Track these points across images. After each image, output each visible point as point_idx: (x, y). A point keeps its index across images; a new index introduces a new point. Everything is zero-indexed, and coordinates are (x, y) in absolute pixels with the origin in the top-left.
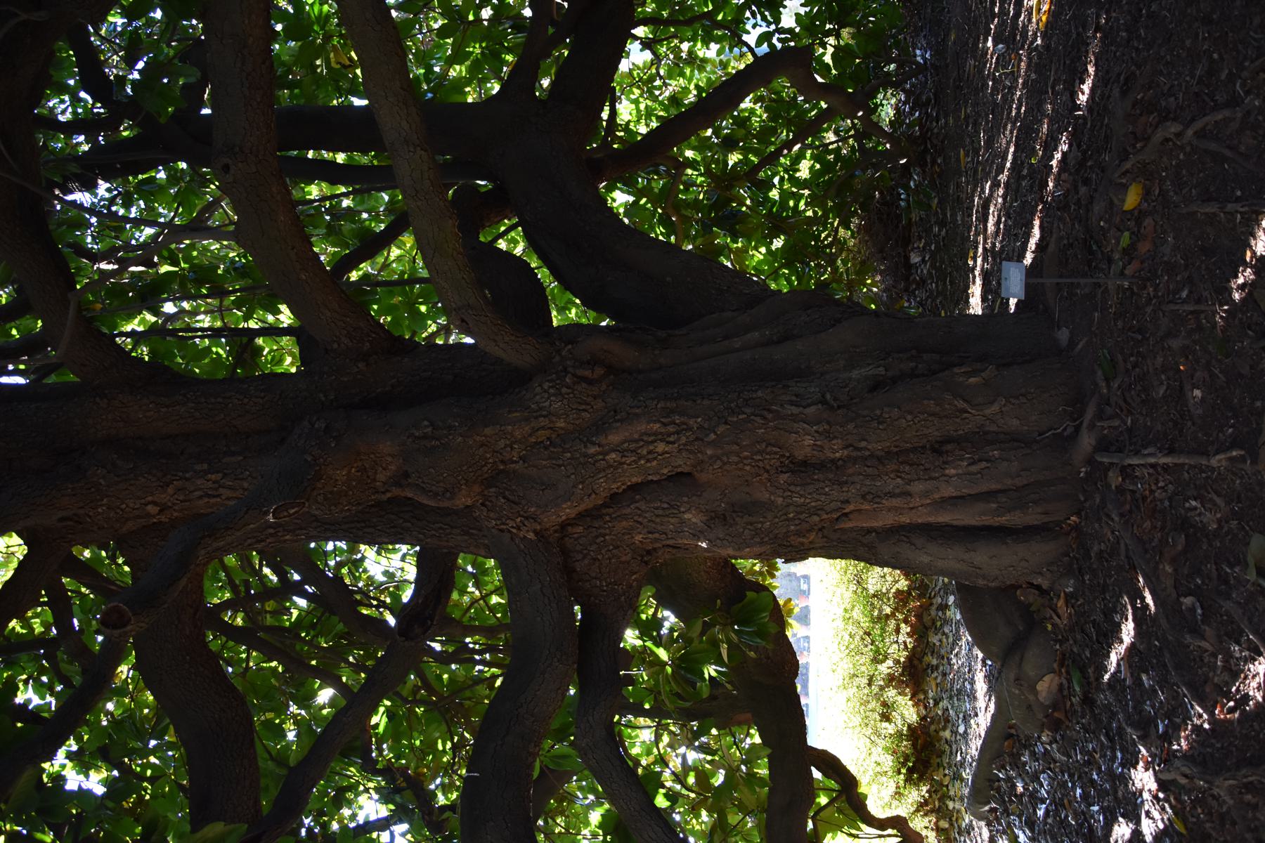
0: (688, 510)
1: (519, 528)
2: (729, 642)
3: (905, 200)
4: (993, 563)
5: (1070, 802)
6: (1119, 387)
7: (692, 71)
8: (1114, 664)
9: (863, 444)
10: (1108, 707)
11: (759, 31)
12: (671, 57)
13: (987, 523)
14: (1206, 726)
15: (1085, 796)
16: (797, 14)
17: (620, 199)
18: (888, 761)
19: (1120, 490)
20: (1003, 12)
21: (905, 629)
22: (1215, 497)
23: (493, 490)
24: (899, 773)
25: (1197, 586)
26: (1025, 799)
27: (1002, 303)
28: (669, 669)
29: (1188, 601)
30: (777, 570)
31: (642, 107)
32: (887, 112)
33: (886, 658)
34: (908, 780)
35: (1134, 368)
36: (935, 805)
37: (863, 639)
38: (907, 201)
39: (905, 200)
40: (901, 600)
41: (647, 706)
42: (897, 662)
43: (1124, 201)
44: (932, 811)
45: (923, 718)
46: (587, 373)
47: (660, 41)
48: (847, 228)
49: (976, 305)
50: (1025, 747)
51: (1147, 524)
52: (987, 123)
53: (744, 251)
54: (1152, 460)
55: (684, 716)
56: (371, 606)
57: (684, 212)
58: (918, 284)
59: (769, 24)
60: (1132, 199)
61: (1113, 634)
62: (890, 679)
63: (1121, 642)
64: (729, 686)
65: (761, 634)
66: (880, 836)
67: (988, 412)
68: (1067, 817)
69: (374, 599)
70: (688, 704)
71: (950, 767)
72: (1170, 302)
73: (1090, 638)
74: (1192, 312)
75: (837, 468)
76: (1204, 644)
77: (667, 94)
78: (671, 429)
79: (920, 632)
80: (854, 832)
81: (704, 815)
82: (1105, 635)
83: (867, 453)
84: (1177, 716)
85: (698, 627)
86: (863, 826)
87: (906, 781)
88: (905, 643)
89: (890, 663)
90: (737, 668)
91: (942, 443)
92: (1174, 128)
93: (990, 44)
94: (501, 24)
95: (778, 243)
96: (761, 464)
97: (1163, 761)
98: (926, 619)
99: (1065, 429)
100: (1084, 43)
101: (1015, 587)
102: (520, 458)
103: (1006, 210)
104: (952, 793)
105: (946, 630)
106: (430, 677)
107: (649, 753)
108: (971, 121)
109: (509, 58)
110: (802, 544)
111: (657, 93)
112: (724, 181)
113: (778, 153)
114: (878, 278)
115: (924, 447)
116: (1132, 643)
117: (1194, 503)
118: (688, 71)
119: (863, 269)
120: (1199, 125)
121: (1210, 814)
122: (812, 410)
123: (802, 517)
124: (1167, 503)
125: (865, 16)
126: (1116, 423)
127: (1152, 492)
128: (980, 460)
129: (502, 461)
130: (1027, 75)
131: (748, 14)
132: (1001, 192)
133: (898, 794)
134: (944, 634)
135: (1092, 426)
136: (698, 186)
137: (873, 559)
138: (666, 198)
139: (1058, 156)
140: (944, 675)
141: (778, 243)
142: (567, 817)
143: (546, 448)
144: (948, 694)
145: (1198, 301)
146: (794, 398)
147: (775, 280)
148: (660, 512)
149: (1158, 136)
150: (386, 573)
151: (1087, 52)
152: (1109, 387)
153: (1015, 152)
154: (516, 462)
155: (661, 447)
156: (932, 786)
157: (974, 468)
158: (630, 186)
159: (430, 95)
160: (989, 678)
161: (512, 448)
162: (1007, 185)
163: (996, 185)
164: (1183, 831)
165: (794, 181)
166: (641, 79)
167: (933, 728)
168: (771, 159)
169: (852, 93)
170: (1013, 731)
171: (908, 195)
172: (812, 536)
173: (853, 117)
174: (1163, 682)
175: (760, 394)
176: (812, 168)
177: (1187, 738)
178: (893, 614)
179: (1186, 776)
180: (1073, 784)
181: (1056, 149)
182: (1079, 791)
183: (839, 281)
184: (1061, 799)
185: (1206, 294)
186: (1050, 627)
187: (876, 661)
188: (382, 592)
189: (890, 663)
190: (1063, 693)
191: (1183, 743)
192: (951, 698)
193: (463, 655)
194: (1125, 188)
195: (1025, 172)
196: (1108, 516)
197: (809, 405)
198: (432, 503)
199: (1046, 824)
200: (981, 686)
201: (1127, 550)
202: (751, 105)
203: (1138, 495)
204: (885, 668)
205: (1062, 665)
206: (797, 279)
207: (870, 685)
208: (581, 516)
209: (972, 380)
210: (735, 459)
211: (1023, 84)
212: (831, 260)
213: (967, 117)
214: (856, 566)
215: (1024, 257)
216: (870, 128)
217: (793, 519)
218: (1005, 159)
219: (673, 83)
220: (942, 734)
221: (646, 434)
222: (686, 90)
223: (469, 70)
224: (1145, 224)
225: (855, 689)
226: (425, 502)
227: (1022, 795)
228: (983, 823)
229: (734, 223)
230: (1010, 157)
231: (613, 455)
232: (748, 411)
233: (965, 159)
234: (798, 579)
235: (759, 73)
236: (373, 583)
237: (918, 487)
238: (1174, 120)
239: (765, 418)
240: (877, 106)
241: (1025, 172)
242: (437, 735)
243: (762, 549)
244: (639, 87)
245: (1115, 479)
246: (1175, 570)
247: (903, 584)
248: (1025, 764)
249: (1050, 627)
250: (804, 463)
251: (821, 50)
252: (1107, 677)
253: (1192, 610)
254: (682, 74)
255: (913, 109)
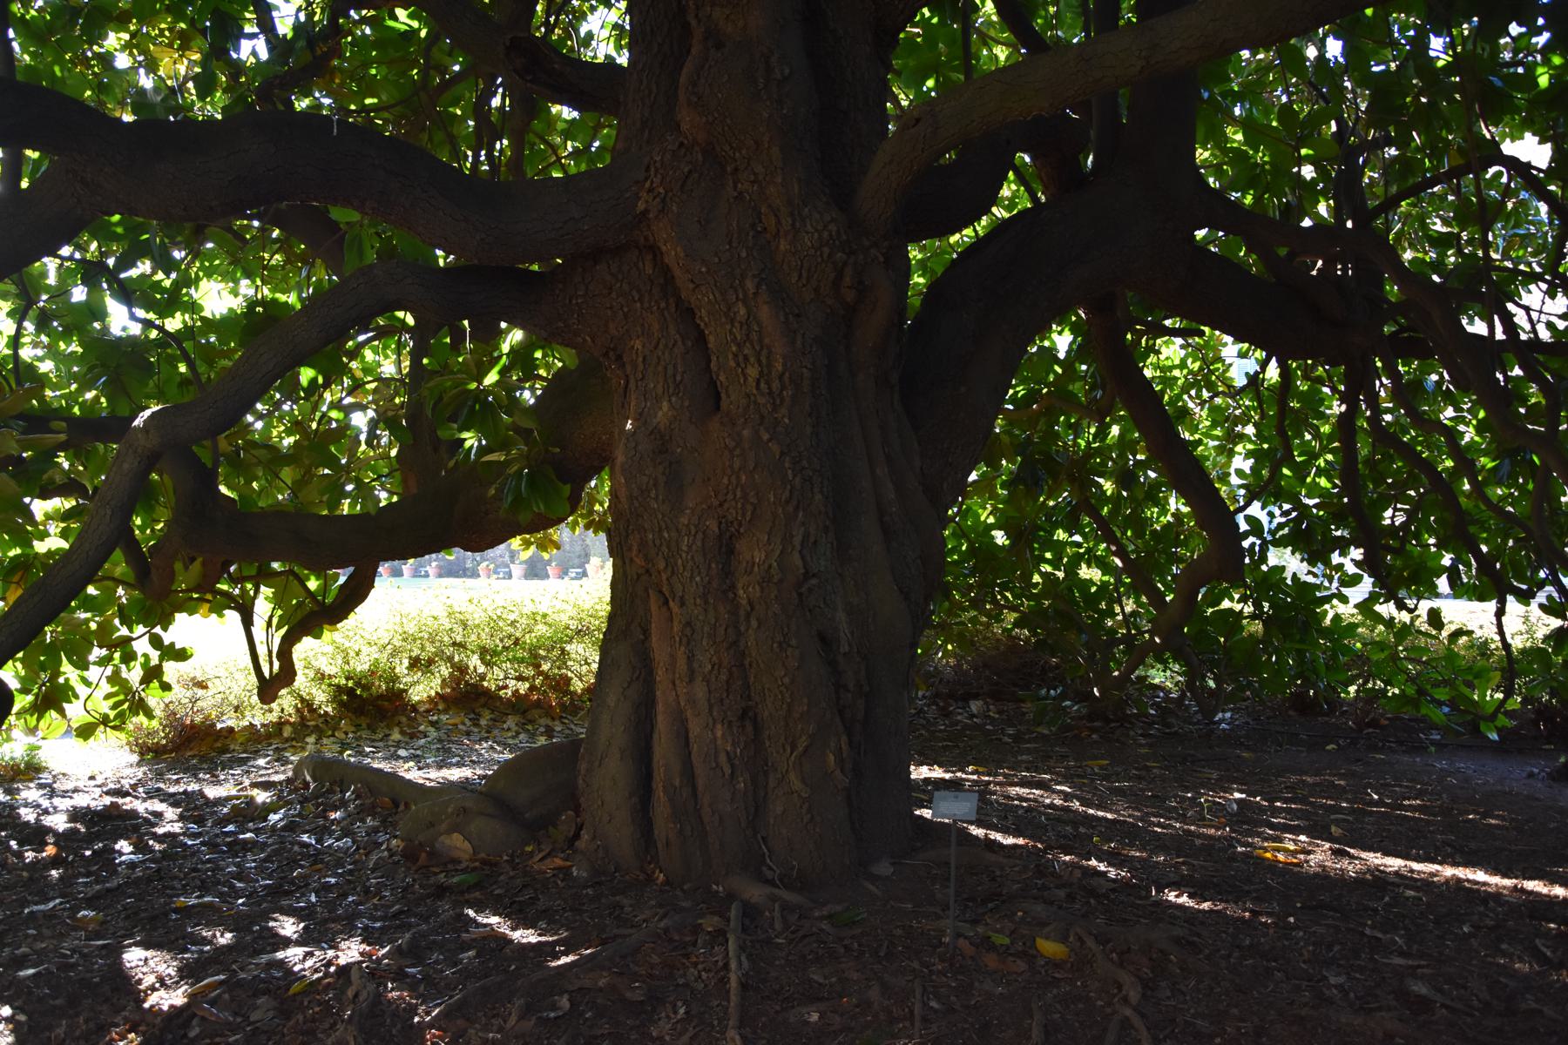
0: (672, 407)
1: (650, 191)
2: (507, 463)
3: (1051, 691)
4: (608, 783)
5: (319, 871)
6: (822, 930)
7: (1217, 438)
8: (485, 921)
9: (754, 623)
10: (435, 913)
11: (1264, 519)
12: (1237, 412)
13: (655, 774)
14: (416, 1019)
15: (327, 887)
16: (1283, 568)
17: (1062, 341)
18: (361, 666)
19: (697, 929)
20: (1276, 812)
21: (523, 687)
22: (688, 1035)
23: (700, 157)
24: (347, 679)
25: (582, 1014)
26: (321, 822)
27: (922, 800)
28: (473, 386)
29: (565, 1003)
30: (595, 532)
31: (1176, 373)
32: (1158, 676)
33: (487, 664)
34: (339, 689)
35: (845, 947)
36: (308, 720)
37: (509, 637)
38: (1047, 697)
39: (1051, 691)
40: (558, 683)
41: (425, 361)
42: (483, 677)
43: (1047, 938)
44: (303, 718)
45: (414, 708)
46: (847, 280)
47: (1258, 397)
48: (1016, 624)
49: (920, 772)
50: (384, 822)
51: (655, 959)
52: (1143, 790)
53: (994, 496)
54: (733, 965)
55: (414, 410)
56: (548, 16)
57: (1043, 420)
58: (944, 709)
59: (1273, 532)
60: (1049, 947)
61: (521, 919)
62: (462, 669)
63: (513, 929)
64: (451, 463)
65: (518, 501)
66: (270, 652)
67: (792, 776)
68: (302, 867)
69: (557, 20)
70: (429, 413)
71: (357, 739)
72: (925, 989)
73: (516, 895)
74: (912, 1012)
75: (725, 592)
76: (513, 1020)
77: (1191, 405)
78: (776, 385)
79: (519, 706)
80: (275, 621)
81: (289, 441)
82: (520, 911)
83: (742, 629)
84: (429, 988)
85: (527, 423)
86: (283, 631)
87: (338, 686)
88: (506, 687)
89: (481, 669)
90: (477, 472)
91: (755, 721)
92: (1134, 995)
93: (1237, 795)
94: (1293, 190)
95: (1000, 537)
96: (730, 496)
97: (374, 973)
98: (535, 713)
99: (770, 868)
100: (1237, 897)
101: (577, 809)
102: (741, 193)
103: (1035, 808)
104: (325, 741)
105: (522, 736)
106: (457, 89)
107: (367, 370)
108: (1143, 773)
109: (1248, 200)
110: (630, 549)
111: (1193, 393)
112: (1080, 471)
113: (1110, 538)
114: (952, 661)
115: (749, 698)
116: (512, 941)
117: (682, 1011)
118: (1218, 432)
119: (963, 640)
120: (1137, 1021)
121: (314, 1020)
122: (796, 559)
123: (664, 548)
124: (681, 981)
125: (1277, 651)
126: (778, 926)
127: (695, 965)
128: (732, 766)
129: (736, 169)
130: (1200, 836)
131: (1286, 507)
132: (1058, 802)
133: (321, 677)
134: (518, 733)
135: (773, 898)
136: (1074, 440)
137: (606, 648)
138: (1061, 400)
139: (1102, 867)
140: (468, 734)
141: (1000, 537)
142: (283, 267)
143: (753, 226)
144: (444, 737)
145: (925, 1020)
146: (812, 539)
147: (953, 534)
148: (670, 371)
149: (1125, 978)
150: (590, 36)
151: (1227, 901)
152: (822, 918)
153: (1106, 819)
154: (735, 188)
155: (753, 372)
156: (333, 718)
157: (723, 758)
158: (1076, 354)
159: (1206, 95)
160: (465, 784)
161: (753, 182)
162: (1067, 810)
163: (1067, 797)
164: (291, 992)
165: (1077, 560)
166: (1212, 372)
167: (404, 719)
168: (1106, 531)
169: (1185, 635)
170: (402, 807)
171: (1054, 698)
172: (639, 561)
173: (1152, 633)
174: (466, 975)
175: (818, 497)
176: (1091, 582)
177: (401, 998)
178: (541, 673)
179: (356, 996)
180: (341, 875)
181: (1110, 865)
182: (333, 880)
183: (950, 613)
184: (322, 861)
185: (934, 1028)
186: (529, 849)
187: (484, 652)
188: (565, 30)
189: (481, 669)
190: (450, 863)
191: (395, 994)
192: (440, 741)
193: (485, 135)
194: (1063, 939)
195: (1082, 830)
196: (665, 916)
197: (803, 558)
198: (683, 79)
199: (292, 844)
200: (455, 774)
201: (625, 936)
202: (1173, 509)
203: (690, 949)
204: (474, 661)
205: (484, 862)
206: (955, 562)
207: (454, 644)
208: (666, 272)
209: (832, 757)
210: (737, 465)
211: (1189, 831)
212: (976, 604)
213: (1148, 769)
214: (599, 630)
215: (979, 826)
216: (1139, 653)
217: (661, 537)
218: (1099, 808)
219: (1204, 413)
220: (396, 730)
221: (770, 352)
222: (1194, 429)
223: (1236, 151)
224: (1019, 962)
225: (448, 626)
226: (685, 70)
227: (326, 818)
228: (290, 774)
229: (1027, 482)
230: (1100, 814)
231: (743, 311)
232: (798, 480)
233: (1096, 765)
234: (582, 566)
235: (1213, 512)
236: (577, 19)
237: (700, 691)
238: (1144, 995)
239: (787, 502)
240: (1164, 662)
241: (1082, 830)
242: (384, 98)
243: (623, 500)
244: (1201, 369)
245: (710, 923)
246: (601, 990)
247: (578, 686)
248: (363, 821)
249: (529, 849)
250: (731, 552)
251: (1237, 596)
252: (471, 913)
253: (554, 1008)
254: (1214, 425)
255: (1156, 706)
